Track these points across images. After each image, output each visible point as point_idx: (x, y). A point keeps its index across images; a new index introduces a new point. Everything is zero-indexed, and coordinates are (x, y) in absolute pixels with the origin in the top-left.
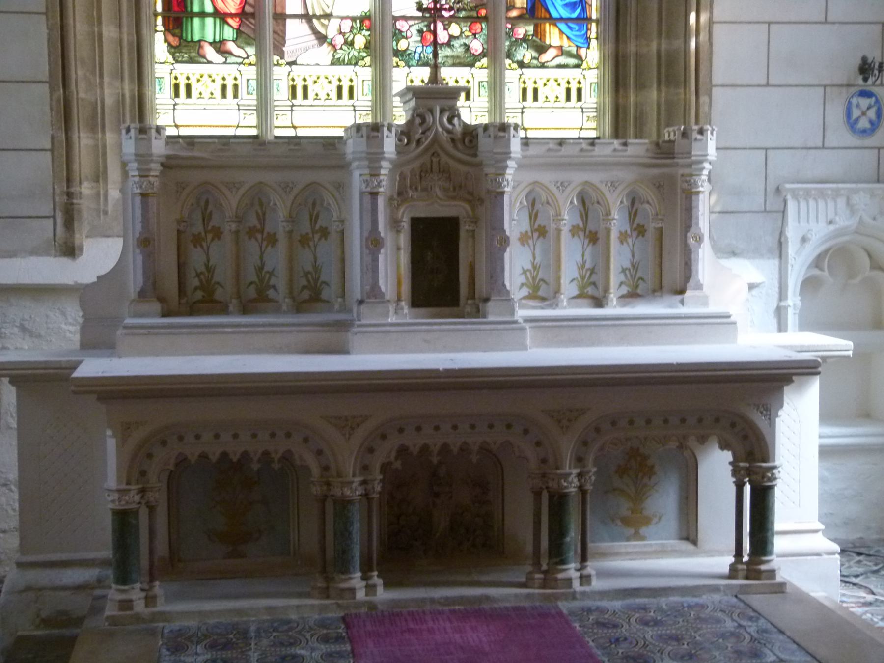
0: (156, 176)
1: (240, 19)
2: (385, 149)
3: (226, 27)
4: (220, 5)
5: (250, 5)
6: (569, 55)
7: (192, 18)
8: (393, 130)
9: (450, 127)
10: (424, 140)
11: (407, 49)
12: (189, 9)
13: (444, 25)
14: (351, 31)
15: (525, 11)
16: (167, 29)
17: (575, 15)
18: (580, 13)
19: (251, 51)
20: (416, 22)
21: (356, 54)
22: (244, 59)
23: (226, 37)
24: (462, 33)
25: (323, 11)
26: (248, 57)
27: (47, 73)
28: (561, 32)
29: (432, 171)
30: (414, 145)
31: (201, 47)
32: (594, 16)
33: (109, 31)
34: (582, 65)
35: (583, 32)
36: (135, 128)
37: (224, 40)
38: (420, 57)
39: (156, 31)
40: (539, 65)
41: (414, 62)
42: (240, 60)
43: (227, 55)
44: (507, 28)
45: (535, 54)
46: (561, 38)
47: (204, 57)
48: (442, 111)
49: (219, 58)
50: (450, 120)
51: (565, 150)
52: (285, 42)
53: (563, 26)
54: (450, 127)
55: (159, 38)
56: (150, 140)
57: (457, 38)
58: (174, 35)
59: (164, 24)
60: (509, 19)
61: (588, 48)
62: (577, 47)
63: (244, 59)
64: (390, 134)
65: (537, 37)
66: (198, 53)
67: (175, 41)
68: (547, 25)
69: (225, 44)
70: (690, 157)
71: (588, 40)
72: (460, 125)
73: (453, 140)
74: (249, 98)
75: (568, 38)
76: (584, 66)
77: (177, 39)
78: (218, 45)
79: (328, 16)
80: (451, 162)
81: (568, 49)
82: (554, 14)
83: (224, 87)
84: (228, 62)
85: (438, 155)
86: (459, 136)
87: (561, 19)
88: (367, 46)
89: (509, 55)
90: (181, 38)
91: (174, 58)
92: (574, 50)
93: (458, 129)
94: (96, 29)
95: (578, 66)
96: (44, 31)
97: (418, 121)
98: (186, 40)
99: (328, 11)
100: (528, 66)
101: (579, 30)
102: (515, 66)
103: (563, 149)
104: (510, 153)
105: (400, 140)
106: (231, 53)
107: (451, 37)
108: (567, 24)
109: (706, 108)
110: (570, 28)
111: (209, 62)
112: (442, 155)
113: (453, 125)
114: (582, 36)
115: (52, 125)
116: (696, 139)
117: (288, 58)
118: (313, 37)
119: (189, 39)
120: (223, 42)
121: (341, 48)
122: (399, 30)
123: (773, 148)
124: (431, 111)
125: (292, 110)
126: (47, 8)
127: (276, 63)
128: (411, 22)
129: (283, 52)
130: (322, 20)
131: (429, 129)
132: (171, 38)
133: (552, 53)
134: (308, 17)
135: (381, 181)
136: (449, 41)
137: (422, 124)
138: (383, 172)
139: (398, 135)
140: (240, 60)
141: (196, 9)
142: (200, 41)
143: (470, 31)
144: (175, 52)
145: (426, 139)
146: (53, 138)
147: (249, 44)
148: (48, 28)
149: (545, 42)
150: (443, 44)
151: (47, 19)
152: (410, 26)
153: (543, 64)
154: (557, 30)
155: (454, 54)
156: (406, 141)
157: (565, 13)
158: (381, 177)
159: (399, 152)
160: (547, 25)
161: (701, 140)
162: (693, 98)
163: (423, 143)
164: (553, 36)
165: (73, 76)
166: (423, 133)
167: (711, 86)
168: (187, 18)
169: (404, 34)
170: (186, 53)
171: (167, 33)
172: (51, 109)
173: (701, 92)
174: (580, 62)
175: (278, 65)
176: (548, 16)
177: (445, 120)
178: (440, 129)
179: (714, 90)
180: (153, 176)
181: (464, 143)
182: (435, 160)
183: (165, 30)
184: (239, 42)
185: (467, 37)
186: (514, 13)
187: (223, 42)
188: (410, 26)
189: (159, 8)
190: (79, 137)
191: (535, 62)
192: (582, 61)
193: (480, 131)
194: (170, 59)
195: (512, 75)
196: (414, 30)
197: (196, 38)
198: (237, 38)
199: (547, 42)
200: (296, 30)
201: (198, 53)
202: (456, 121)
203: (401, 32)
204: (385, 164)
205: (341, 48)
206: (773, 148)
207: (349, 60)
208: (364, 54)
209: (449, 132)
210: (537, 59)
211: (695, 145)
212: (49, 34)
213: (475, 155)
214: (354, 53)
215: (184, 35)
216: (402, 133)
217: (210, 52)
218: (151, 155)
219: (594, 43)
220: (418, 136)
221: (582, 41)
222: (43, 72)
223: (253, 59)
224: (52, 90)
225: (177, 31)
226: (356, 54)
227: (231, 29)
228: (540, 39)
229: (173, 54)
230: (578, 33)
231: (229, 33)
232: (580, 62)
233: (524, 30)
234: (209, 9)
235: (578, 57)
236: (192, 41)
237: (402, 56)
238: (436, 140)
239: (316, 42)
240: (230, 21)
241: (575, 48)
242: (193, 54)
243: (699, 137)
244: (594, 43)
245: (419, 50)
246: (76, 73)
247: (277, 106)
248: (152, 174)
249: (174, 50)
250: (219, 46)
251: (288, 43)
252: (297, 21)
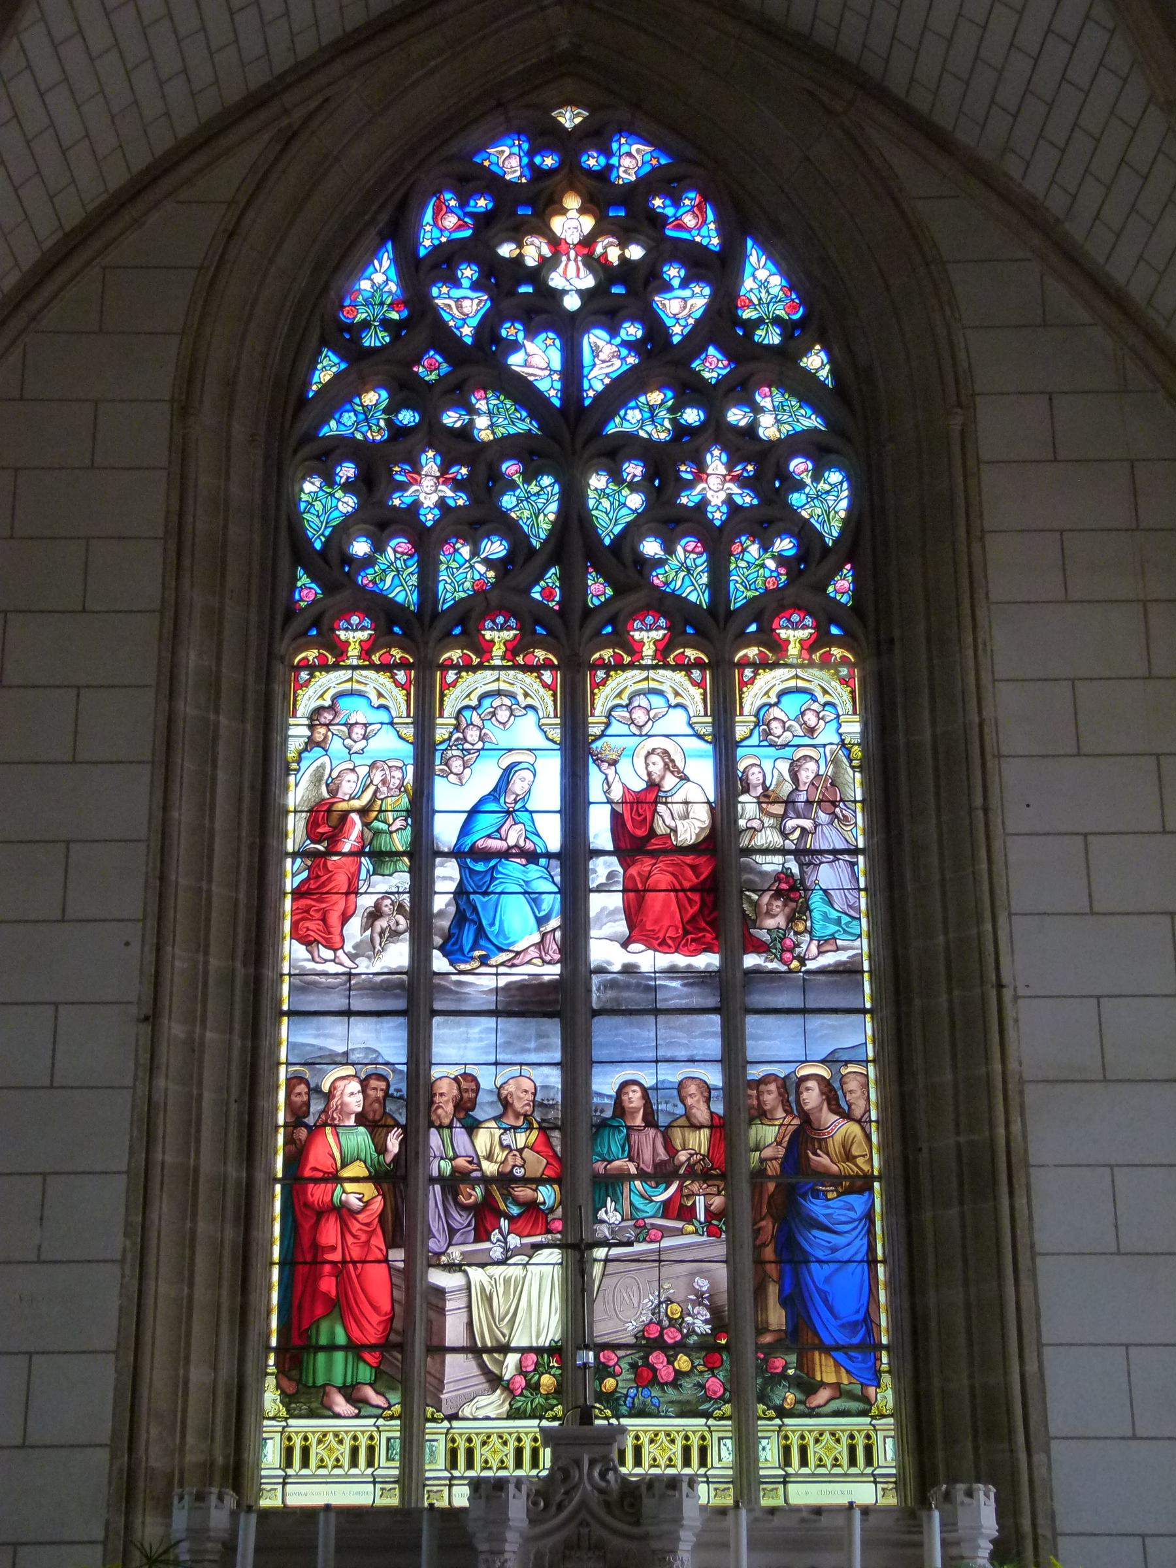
0: (215, 1561)
1: (381, 1354)
2: (511, 1515)
3: (362, 1365)
4: (356, 1334)
5: (397, 1333)
6: (851, 1396)
7: (315, 1354)
8: (524, 1488)
9: (603, 1484)
10: (566, 1503)
11: (615, 1391)
12: (314, 1341)
13: (667, 1356)
14: (535, 1370)
15: (783, 1335)
16: (283, 1371)
17: (856, 1340)
18: (864, 1337)
19: (395, 1397)
20: (629, 1352)
21: (542, 1401)
22: (385, 1409)
23: (361, 1379)
24: (693, 1367)
25: (497, 1340)
26: (389, 1408)
27: (109, 1433)
28: (837, 1364)
29: (579, 1547)
30: (553, 1509)
31: (325, 1394)
32: (884, 1341)
33: (198, 1374)
34: (870, 1411)
35: (870, 1364)
36: (190, 1494)
37: (358, 1383)
38: (633, 1403)
39: (267, 1374)
40: (807, 1411)
41: (624, 1410)
42: (379, 1411)
43: (360, 1405)
44: (758, 1358)
45: (800, 1396)
46: (837, 1372)
47: (330, 1409)
48: (592, 1463)
49: (351, 1410)
50: (603, 1475)
51: (777, 1521)
52: (443, 1388)
53: (839, 1356)
54: (603, 1484)
55: (271, 1381)
56: (209, 1508)
57: (686, 1374)
58: (290, 1379)
59: (276, 1364)
60: (759, 1347)
61: (878, 1386)
62: (862, 1384)
63: (385, 1409)
64: (518, 1494)
65: (802, 1371)
66: (322, 1403)
67: (291, 1388)
68: (817, 1354)
69: (359, 1390)
70: (956, 1531)
71: (877, 1374)
72: (616, 1481)
73: (607, 1505)
74: (389, 1468)
75: (848, 1372)
76: (874, 1411)
77: (294, 1384)
78: (349, 1391)
79: (505, 1349)
80: (605, 1534)
81: (848, 1388)
82: (828, 1340)
83: (355, 1451)
84: (362, 1413)
85: (588, 1525)
86: (615, 1496)
87: (838, 1348)
88: (559, 1391)
89: (762, 1398)
90: (299, 1382)
91: (288, 1411)
92: (857, 1389)
93: (614, 1485)
94: (181, 1372)
95: (863, 1413)
96: (111, 1375)
97: (560, 1476)
98: (305, 1386)
99: (504, 1341)
100: (791, 1414)
101: (864, 1361)
102: (772, 1413)
103: (775, 1518)
104: (682, 1518)
105: (535, 1504)
106: (366, 1402)
107: (679, 1374)
108: (846, 1354)
109: (1044, 1471)
110: (850, 1358)
111: (337, 1416)
112: (595, 1526)
113: (608, 1482)
114: (870, 1368)
115: (108, 1506)
116: (962, 1503)
117: (447, 1410)
118: (482, 1379)
119: (310, 1384)
120: (356, 1385)
121: (521, 1394)
122: (603, 1364)
123: (1153, 1535)
124: (578, 1463)
125: (450, 1486)
126: (118, 1344)
127: (429, 1416)
128: (621, 1353)
129: (440, 1401)
130: (496, 1355)
131: (575, 1488)
132: (285, 1383)
133: (823, 1395)
134: (473, 1350)
135: (506, 1561)
136: (676, 1379)
137: (564, 1480)
138: (508, 1547)
139: (532, 1497)
140: (379, 1411)
141: (323, 1341)
142: (324, 1386)
143: (704, 1365)
144: (290, 1403)
145: (570, 1502)
146: (107, 1524)
147: (392, 1389)
148: (116, 1371)
149: (814, 1378)
150: (667, 1383)
151: (117, 1359)
152: (619, 1358)
153: (813, 1409)
154: (831, 1362)
155: (681, 1398)
156: (542, 1504)
157: (842, 1338)
158: (507, 1556)
159: (533, 1521)
160: (817, 1354)
161: (970, 1505)
162: (1023, 1456)
163: (566, 1507)
164: (826, 1371)
165: (144, 1436)
166: (566, 1493)
167: (1048, 1439)
168: (308, 1354)
169: (611, 1370)
170: (305, 1404)
171: (280, 1376)
172: (110, 1483)
173: (1035, 1445)
174: (867, 1407)
175: (433, 1420)
176: (817, 1341)
177: (596, 1474)
178: (589, 1487)
179: (1054, 1445)
180: (210, 1561)
181: (622, 1506)
182: (585, 1531)
183: (279, 1372)
184: (378, 1386)
185: (702, 1372)
186: (768, 1339)
187: (356, 1385)
188: (619, 1358)
189: (274, 1342)
190: (143, 1523)
191: (801, 1407)
192: (871, 1405)
193: (644, 1489)
194: (284, 1413)
195: (767, 1428)
196: (624, 1365)
197: (320, 1381)
198: (375, 1381)
199: (818, 1378)
200: (457, 1367)
201: (322, 1403)
202: (611, 1476)
203: (606, 1366)
204: (511, 1536)
205: (521, 1394)
206: (1153, 1535)
207: (533, 1410)
208: (555, 1402)
209: (602, 1491)
210: (803, 1403)
211: (960, 1511)
212: (117, 1379)
213: (637, 1523)
214: (539, 1400)
215: (304, 1378)
216: (538, 1493)
217: (341, 1404)
218: (208, 1530)
219: (886, 1379)
220: (559, 1497)
221: (869, 1376)
222: (104, 1433)
223: (397, 1409)
224: (113, 1457)
225: (294, 1373)
226: (542, 1401)
227: (368, 1369)
228: (807, 1374)
229: (286, 1405)
230: (863, 1365)
231: (365, 1373)
232: (867, 1407)
233: (786, 1363)
234: (341, 1339)
235: (865, 1399)
236: (314, 1386)
237: (608, 1402)
238: (583, 1504)
239: (486, 1386)
240: (367, 1356)
241: (859, 1387)
242: (314, 1405)
243: (967, 1500)
244: (886, 1379)
245: (632, 1392)
246: (148, 1432)
247: (429, 1479)
248: (208, 1557)
249: (288, 1399)
250: (351, 1393)
251: (447, 1388)
252: (461, 1357)
